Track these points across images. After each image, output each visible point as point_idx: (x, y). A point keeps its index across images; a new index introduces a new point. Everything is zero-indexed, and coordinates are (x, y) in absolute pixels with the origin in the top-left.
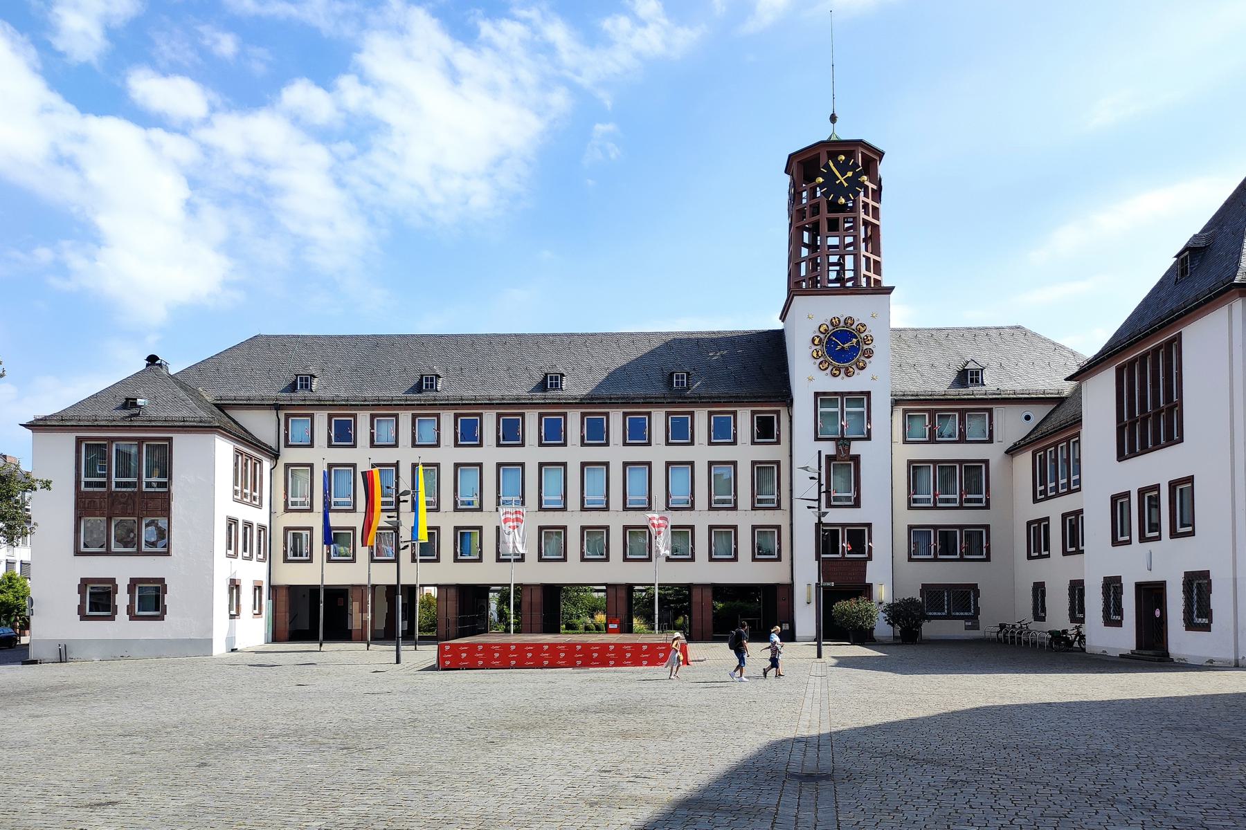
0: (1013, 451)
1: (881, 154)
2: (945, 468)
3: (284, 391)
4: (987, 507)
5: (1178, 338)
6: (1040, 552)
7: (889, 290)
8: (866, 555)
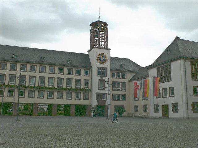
0: (130, 81)
1: (108, 25)
5: (170, 64)
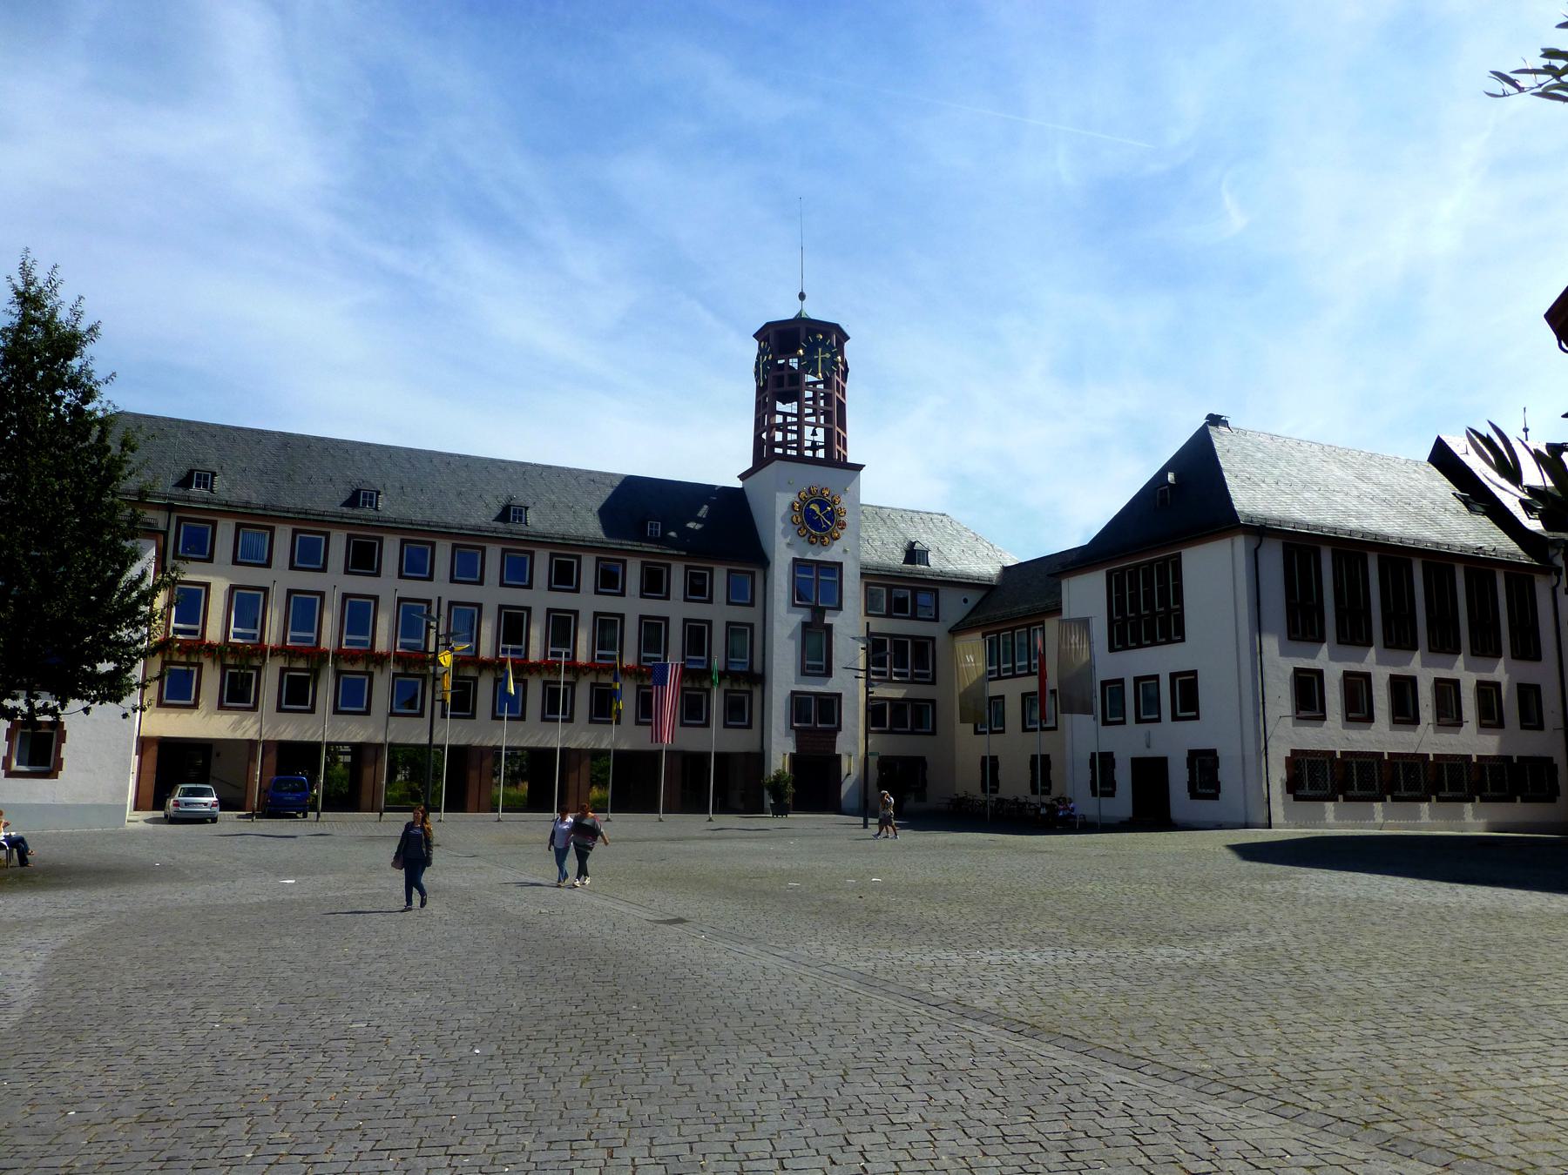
1: (848, 338)
2: (899, 643)
3: (345, 504)
4: (933, 682)
5: (1179, 556)
7: (859, 467)
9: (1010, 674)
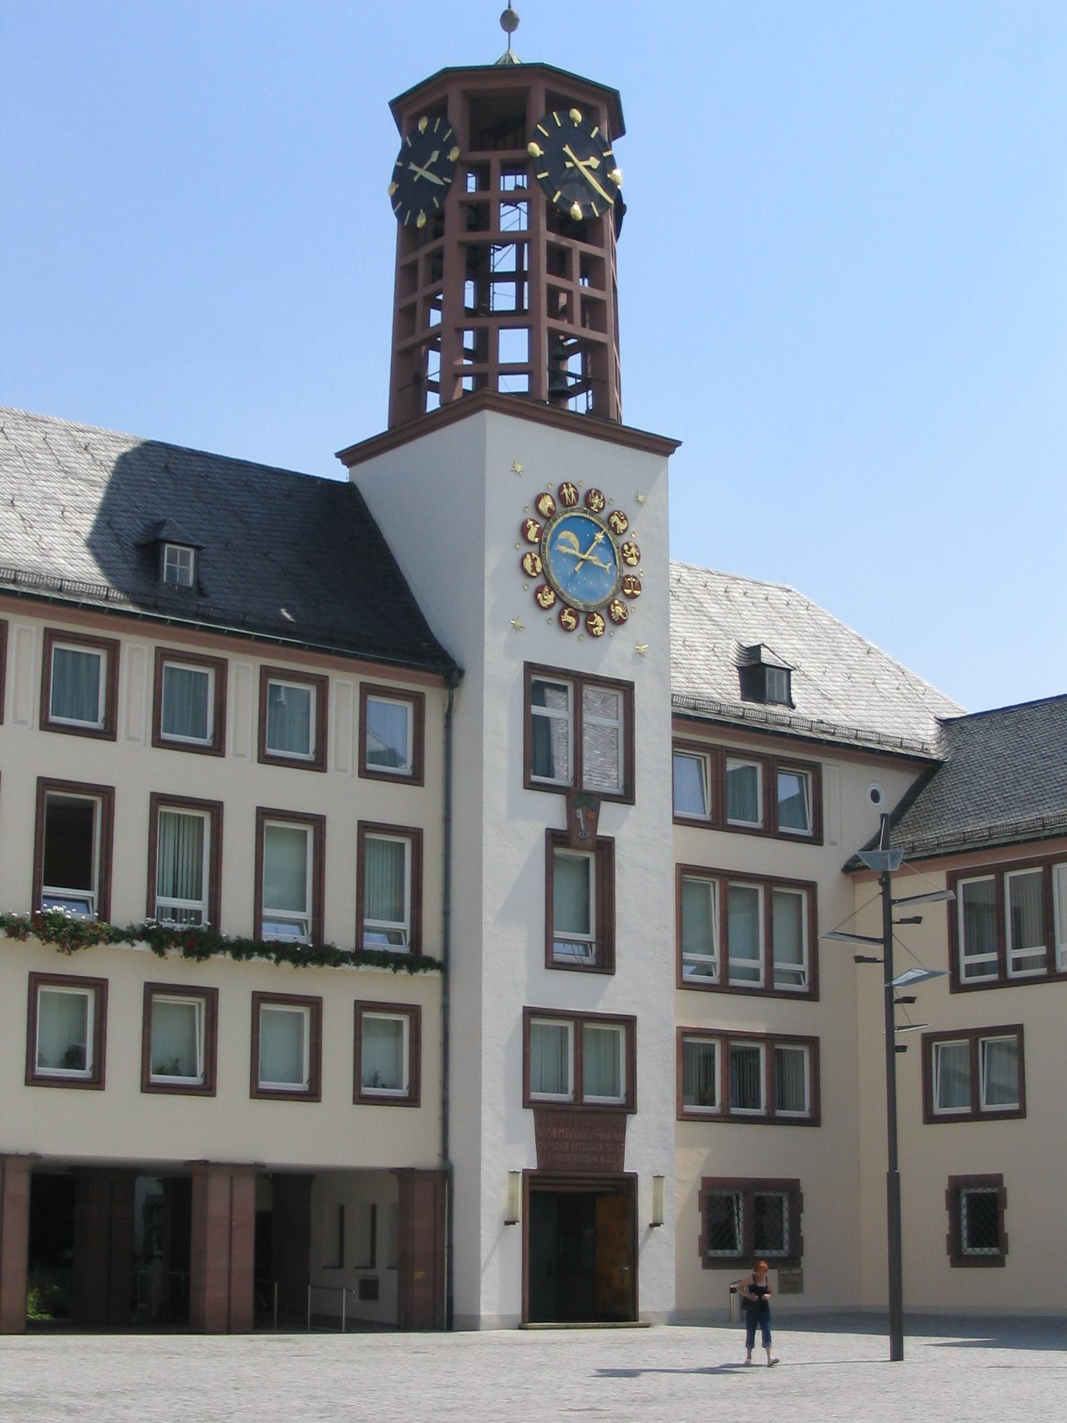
6: (975, 1102)
7: (664, 447)
8: (620, 1099)
9: (994, 977)
